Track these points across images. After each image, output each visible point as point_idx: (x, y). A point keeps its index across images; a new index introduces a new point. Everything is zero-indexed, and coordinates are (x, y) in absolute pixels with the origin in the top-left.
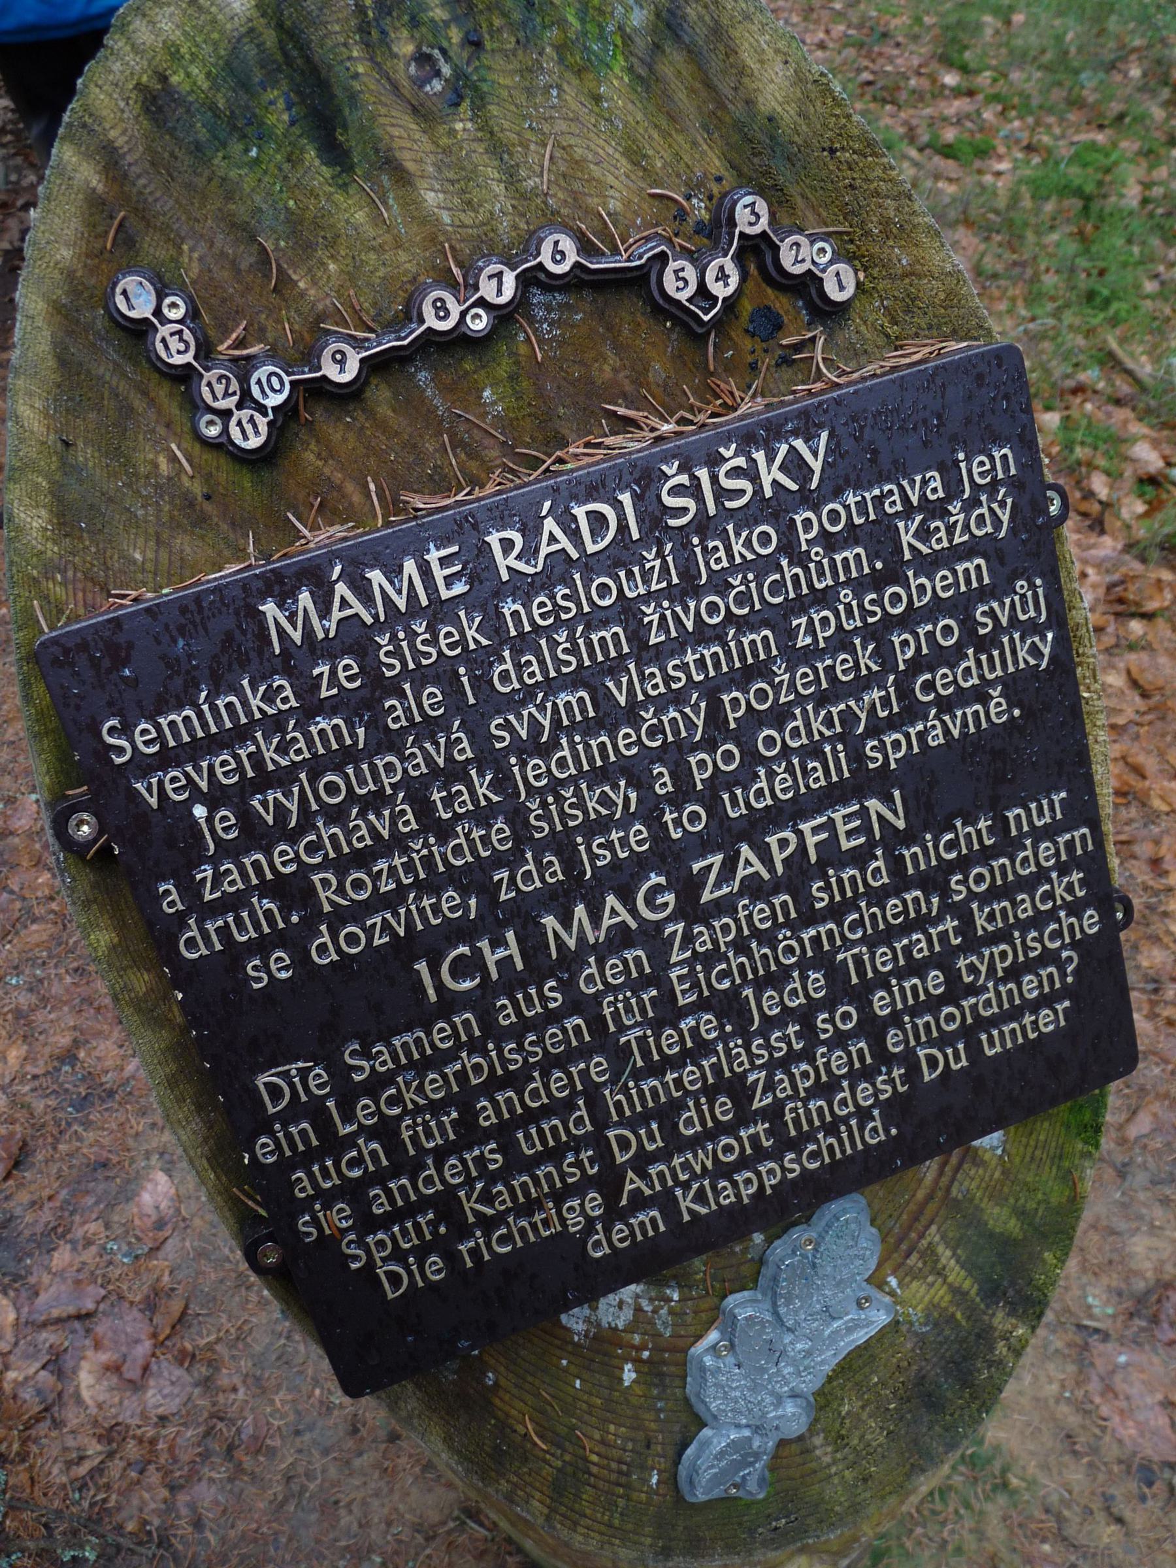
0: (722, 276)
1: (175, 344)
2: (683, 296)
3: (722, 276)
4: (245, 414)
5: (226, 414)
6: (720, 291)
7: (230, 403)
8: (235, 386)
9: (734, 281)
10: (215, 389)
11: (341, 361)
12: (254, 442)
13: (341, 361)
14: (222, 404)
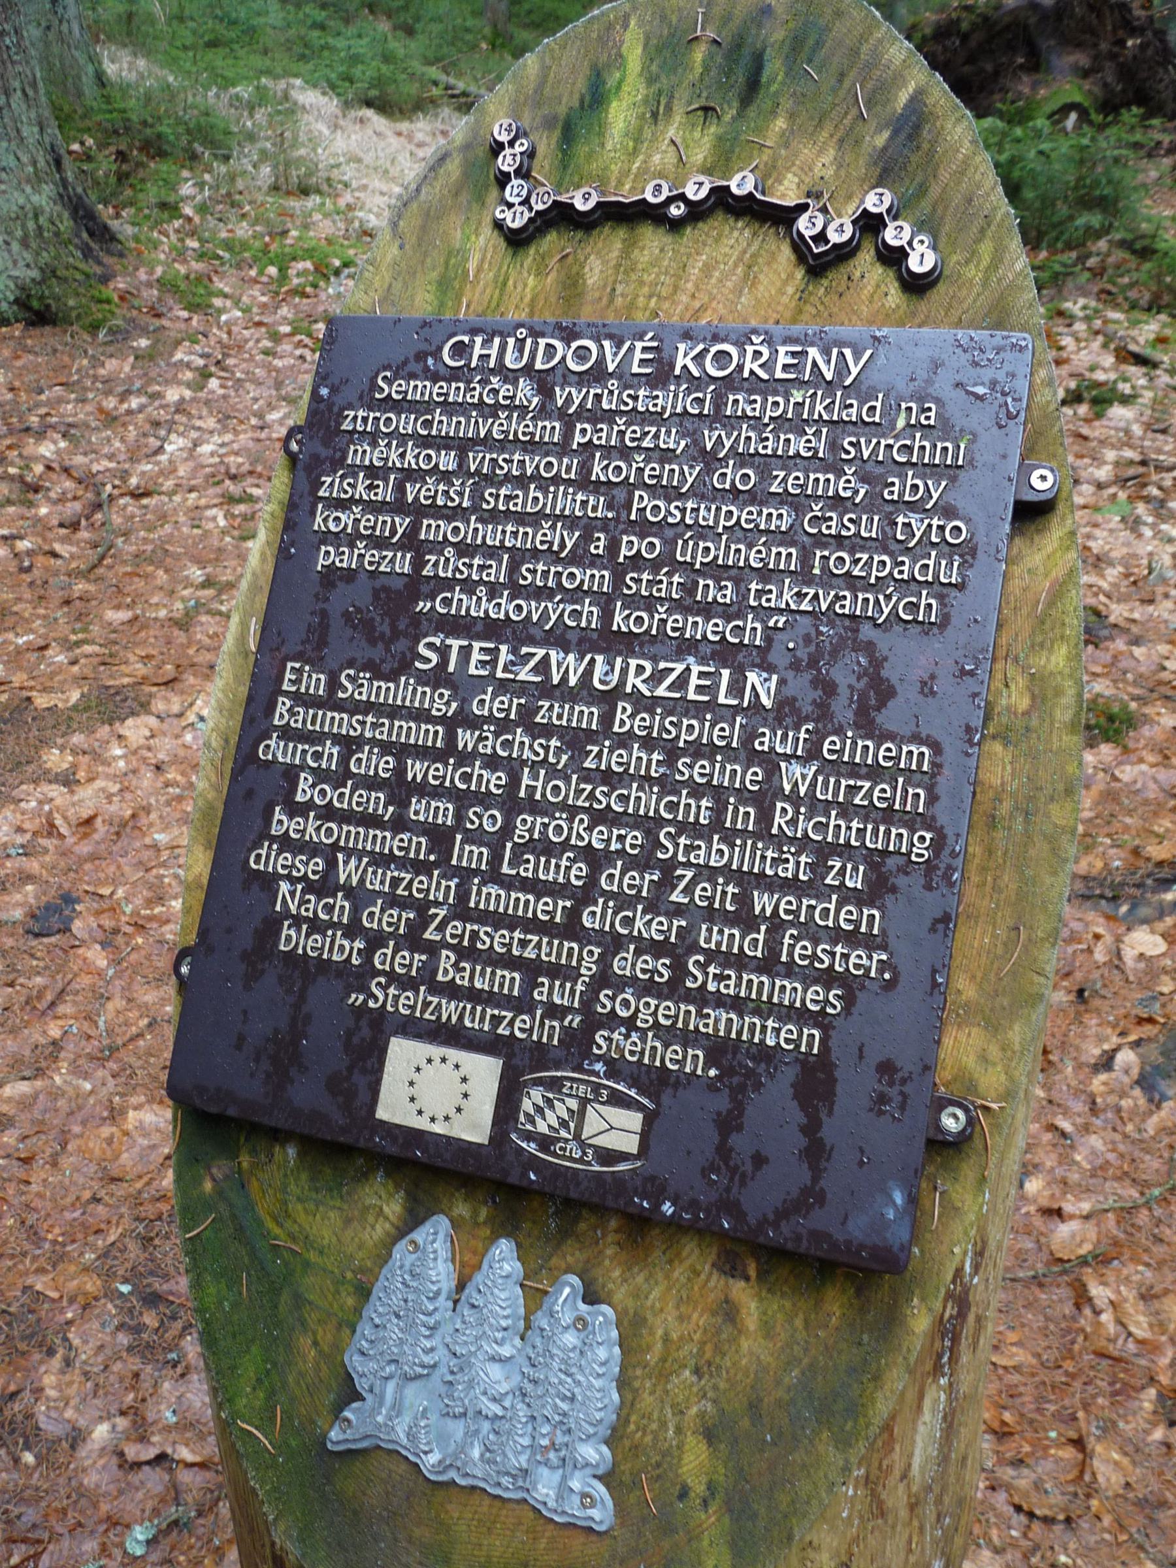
0: (841, 229)
1: (509, 159)
2: (808, 234)
3: (841, 229)
4: (524, 208)
5: (510, 206)
6: (834, 238)
7: (516, 200)
8: (524, 193)
9: (846, 237)
10: (515, 190)
11: (586, 199)
12: (516, 225)
13: (586, 199)
14: (511, 200)
